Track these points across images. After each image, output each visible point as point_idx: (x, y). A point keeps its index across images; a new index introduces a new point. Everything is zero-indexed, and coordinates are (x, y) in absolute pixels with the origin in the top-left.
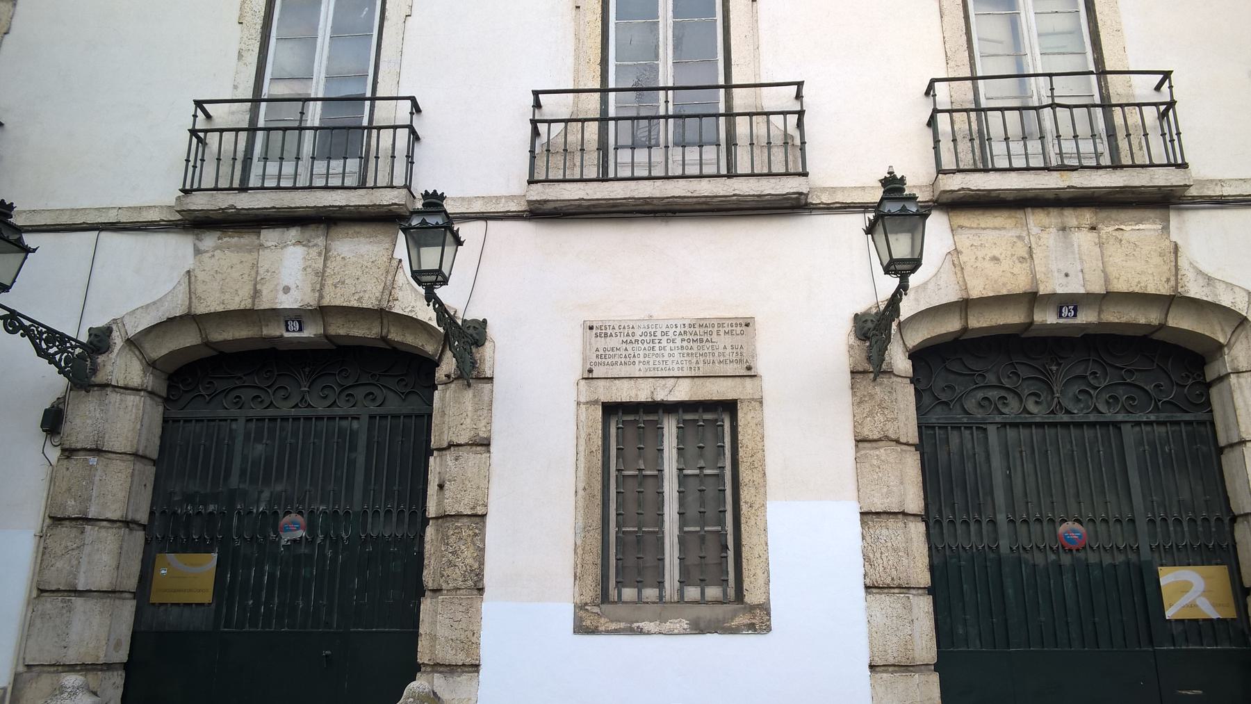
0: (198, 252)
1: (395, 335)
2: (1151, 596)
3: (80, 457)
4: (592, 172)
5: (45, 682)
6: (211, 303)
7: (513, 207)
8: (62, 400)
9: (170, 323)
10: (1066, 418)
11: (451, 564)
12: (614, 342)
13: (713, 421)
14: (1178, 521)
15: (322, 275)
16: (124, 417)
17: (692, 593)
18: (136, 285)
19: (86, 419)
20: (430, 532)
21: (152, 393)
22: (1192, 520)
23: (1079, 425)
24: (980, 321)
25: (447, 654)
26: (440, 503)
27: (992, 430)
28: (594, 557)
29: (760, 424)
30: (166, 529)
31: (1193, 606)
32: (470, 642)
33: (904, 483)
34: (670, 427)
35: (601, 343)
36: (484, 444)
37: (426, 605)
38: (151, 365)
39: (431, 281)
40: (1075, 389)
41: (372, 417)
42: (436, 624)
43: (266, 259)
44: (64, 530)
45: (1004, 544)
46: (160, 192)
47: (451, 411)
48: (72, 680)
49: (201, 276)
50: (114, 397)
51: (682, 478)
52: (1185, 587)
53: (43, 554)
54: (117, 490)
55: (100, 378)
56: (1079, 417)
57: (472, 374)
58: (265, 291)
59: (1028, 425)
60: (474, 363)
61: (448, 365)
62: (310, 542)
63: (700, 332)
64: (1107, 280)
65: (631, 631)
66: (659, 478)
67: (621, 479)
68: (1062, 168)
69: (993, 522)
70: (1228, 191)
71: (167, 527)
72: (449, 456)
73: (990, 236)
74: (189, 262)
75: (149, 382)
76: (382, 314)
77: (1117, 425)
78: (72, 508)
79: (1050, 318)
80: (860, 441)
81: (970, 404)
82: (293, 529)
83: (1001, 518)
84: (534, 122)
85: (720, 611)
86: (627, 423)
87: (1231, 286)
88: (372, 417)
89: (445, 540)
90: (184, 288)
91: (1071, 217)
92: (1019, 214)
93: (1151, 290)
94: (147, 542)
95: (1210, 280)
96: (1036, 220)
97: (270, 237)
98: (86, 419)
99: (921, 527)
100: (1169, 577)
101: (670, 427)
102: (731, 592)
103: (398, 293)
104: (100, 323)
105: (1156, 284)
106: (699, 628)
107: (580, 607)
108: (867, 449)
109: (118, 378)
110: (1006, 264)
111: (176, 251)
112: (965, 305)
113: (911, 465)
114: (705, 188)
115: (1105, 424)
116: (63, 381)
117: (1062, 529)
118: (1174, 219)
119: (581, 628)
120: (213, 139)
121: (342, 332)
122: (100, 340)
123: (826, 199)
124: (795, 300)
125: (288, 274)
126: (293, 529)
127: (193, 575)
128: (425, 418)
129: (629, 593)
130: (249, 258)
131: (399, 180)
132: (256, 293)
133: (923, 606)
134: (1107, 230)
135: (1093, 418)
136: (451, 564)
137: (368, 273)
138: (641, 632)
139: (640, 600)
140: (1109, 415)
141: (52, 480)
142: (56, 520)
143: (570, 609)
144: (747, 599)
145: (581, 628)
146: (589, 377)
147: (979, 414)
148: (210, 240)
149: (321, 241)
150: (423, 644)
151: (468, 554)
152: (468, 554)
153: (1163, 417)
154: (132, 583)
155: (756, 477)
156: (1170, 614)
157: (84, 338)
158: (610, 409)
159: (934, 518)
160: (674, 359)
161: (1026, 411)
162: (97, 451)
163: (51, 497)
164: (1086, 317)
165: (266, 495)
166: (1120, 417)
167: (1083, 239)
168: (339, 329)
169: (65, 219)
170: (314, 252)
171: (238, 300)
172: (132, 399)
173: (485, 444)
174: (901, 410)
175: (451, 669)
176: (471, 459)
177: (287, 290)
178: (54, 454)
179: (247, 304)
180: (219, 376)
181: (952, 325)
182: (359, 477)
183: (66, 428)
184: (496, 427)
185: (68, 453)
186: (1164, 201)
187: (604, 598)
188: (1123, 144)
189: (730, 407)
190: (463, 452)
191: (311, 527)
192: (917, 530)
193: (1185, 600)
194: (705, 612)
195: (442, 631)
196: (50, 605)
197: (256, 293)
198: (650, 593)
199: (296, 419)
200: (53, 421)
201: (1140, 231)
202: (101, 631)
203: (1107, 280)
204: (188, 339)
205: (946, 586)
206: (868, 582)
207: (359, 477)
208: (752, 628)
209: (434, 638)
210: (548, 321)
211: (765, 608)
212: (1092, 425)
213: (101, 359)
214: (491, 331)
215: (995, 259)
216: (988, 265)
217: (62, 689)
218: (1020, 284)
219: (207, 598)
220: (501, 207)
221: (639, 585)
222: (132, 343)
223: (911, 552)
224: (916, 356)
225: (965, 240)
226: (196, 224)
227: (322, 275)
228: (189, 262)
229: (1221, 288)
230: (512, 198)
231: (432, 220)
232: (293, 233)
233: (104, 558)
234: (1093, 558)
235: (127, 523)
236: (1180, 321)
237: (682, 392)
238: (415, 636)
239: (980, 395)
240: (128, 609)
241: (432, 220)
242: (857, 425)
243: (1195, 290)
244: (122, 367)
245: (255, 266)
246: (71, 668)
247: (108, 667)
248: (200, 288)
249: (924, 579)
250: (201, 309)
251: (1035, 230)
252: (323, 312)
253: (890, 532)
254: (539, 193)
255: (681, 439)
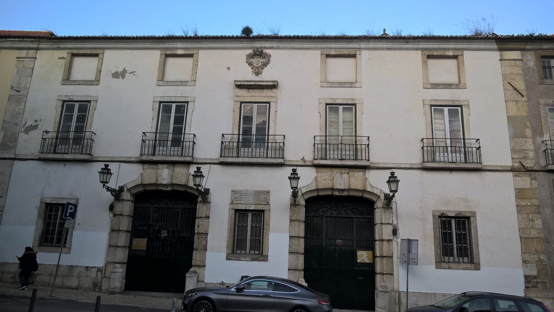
0: (143, 169)
1: (189, 190)
2: (355, 257)
3: (118, 216)
4: (235, 155)
5: (112, 266)
6: (147, 182)
7: (216, 162)
8: (113, 203)
9: (137, 186)
10: (341, 216)
11: (200, 244)
12: (238, 195)
13: (259, 215)
14: (363, 241)
15: (172, 176)
16: (126, 207)
17: (252, 252)
18: (128, 176)
19: (119, 208)
20: (195, 236)
21: (132, 201)
22: (366, 241)
23: (344, 217)
24: (321, 193)
25: (199, 263)
26: (198, 230)
27: (324, 218)
28: (231, 243)
29: (269, 216)
30: (135, 233)
31: (363, 260)
32: (204, 261)
33: (301, 230)
34: (250, 215)
35: (235, 195)
36: (208, 217)
37: (194, 252)
38: (132, 195)
39: (200, 202)
40: (344, 209)
41: (183, 208)
42: (196, 256)
43: (159, 172)
44: (115, 233)
45: (324, 245)
46: (134, 153)
47: (201, 209)
48: (118, 265)
49: (144, 175)
50: (125, 203)
51: (252, 227)
52: (363, 255)
53: (110, 238)
54: (125, 224)
55: (122, 198)
56: (344, 215)
57: (206, 201)
58: (159, 179)
59: (332, 217)
60: (206, 199)
61: (200, 199)
62: (168, 237)
63: (258, 194)
64: (349, 186)
65: (238, 260)
66: (247, 226)
67: (239, 226)
68: (342, 159)
69: (322, 239)
70: (380, 166)
71: (135, 232)
72: (200, 220)
73: (325, 174)
74: (141, 171)
75: (132, 199)
76: (186, 186)
77: (353, 218)
78: (116, 228)
79: (337, 194)
80: (291, 220)
81: (320, 212)
82: (164, 234)
83: (324, 238)
84: (222, 142)
85: (257, 256)
86: (240, 214)
87: (377, 188)
88: (183, 208)
89: (199, 238)
90: (140, 177)
91: (343, 170)
92: (332, 169)
93: (359, 189)
94: (131, 235)
95: (372, 187)
96: (335, 171)
97: (160, 166)
98: (119, 208)
99: (303, 240)
100: (359, 253)
101: (250, 215)
102: (261, 252)
103: (189, 181)
104: (121, 185)
105: (360, 187)
106: (253, 260)
107: (227, 254)
108: (292, 222)
109: (125, 198)
110: (327, 181)
111: (138, 168)
112: (317, 190)
113: (302, 226)
114: (260, 160)
115: (350, 218)
116: (113, 198)
117: (337, 241)
118: (367, 171)
119: (227, 259)
120: (147, 142)
121: (176, 189)
122: (121, 189)
123: (288, 163)
124: (276, 188)
125: (165, 176)
126: (164, 234)
127: (141, 244)
128: (195, 209)
129: (238, 252)
130: (155, 171)
131: (190, 155)
132: (157, 180)
133: (302, 257)
134: (351, 174)
135: (347, 216)
136: (200, 244)
137: (182, 176)
138: (240, 260)
139: (241, 253)
140: (351, 215)
141: (112, 221)
142: (113, 230)
143: (226, 254)
144: (264, 254)
145: (227, 259)
146: (232, 203)
147: (322, 214)
148: (146, 166)
149: (172, 168)
150: (193, 261)
151: (204, 242)
152: (204, 242)
153: (363, 216)
154: (128, 245)
155: (268, 228)
156: (358, 261)
157: (117, 189)
158: (236, 210)
159: (306, 238)
160: (251, 200)
161: (332, 214)
162: (121, 215)
163: (112, 226)
164: (345, 194)
165: (158, 226)
166: (353, 216)
167: (345, 176)
168: (176, 188)
169: (112, 159)
170: (170, 170)
171: (153, 181)
172: (128, 203)
173: (208, 217)
174: (302, 214)
175: (199, 266)
176: (205, 221)
177: (164, 179)
178: (112, 215)
179: (155, 182)
180: (147, 198)
181: (315, 194)
182: (179, 223)
183: (114, 209)
184: (211, 213)
185: (115, 215)
186: (365, 168)
187: (233, 252)
188: (359, 153)
189: (263, 211)
190: (203, 219)
191: (168, 233)
192: (302, 241)
193: (362, 258)
194: (254, 256)
195: (198, 258)
196: (112, 249)
197: (157, 180)
198: (243, 252)
199: (165, 208)
200: (111, 208)
201: (359, 174)
202: (122, 255)
203: (349, 186)
204: (141, 189)
205: (308, 253)
206: (292, 250)
207: (179, 223)
208: (264, 260)
209: (196, 259)
210: (223, 188)
211: (267, 256)
212: (347, 218)
213: (122, 194)
214: (211, 191)
215: (325, 180)
216: (323, 181)
217: (116, 267)
218: (330, 186)
219: (145, 249)
220: (214, 162)
221: (241, 250)
222: (128, 190)
223: (301, 245)
224: (307, 201)
225: (319, 174)
226: (143, 162)
227: (172, 176)
228: (141, 171)
229: (375, 189)
230: (216, 159)
231: (198, 174)
232: (166, 166)
233: (123, 239)
234: (343, 248)
235: (128, 231)
236: (366, 196)
237: (252, 208)
238: (192, 259)
239: (322, 209)
240: (127, 250)
241: (198, 174)
242: (290, 217)
243: (369, 189)
244: (126, 195)
245: (157, 173)
246: (117, 263)
247: (124, 263)
248: (144, 178)
249: (303, 251)
250: (144, 183)
251: (335, 173)
252: (172, 185)
253: (296, 241)
254: (222, 160)
255: (252, 218)
